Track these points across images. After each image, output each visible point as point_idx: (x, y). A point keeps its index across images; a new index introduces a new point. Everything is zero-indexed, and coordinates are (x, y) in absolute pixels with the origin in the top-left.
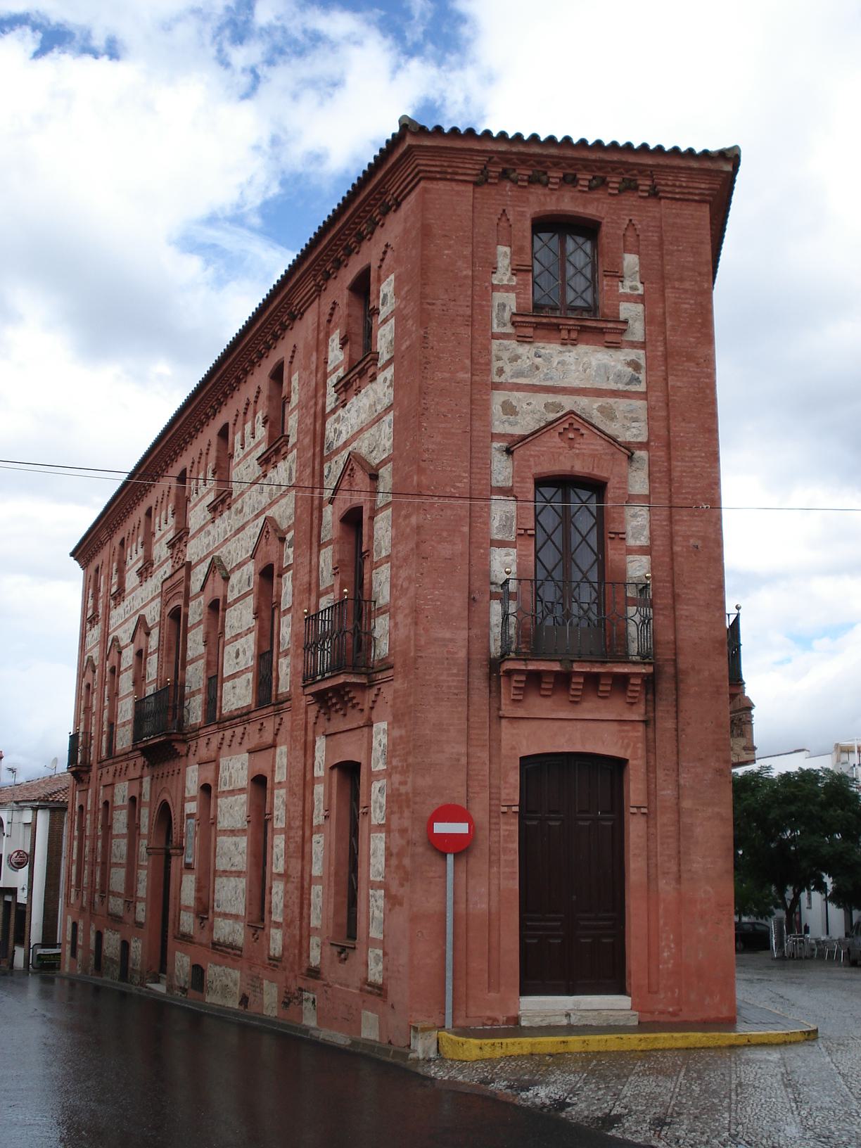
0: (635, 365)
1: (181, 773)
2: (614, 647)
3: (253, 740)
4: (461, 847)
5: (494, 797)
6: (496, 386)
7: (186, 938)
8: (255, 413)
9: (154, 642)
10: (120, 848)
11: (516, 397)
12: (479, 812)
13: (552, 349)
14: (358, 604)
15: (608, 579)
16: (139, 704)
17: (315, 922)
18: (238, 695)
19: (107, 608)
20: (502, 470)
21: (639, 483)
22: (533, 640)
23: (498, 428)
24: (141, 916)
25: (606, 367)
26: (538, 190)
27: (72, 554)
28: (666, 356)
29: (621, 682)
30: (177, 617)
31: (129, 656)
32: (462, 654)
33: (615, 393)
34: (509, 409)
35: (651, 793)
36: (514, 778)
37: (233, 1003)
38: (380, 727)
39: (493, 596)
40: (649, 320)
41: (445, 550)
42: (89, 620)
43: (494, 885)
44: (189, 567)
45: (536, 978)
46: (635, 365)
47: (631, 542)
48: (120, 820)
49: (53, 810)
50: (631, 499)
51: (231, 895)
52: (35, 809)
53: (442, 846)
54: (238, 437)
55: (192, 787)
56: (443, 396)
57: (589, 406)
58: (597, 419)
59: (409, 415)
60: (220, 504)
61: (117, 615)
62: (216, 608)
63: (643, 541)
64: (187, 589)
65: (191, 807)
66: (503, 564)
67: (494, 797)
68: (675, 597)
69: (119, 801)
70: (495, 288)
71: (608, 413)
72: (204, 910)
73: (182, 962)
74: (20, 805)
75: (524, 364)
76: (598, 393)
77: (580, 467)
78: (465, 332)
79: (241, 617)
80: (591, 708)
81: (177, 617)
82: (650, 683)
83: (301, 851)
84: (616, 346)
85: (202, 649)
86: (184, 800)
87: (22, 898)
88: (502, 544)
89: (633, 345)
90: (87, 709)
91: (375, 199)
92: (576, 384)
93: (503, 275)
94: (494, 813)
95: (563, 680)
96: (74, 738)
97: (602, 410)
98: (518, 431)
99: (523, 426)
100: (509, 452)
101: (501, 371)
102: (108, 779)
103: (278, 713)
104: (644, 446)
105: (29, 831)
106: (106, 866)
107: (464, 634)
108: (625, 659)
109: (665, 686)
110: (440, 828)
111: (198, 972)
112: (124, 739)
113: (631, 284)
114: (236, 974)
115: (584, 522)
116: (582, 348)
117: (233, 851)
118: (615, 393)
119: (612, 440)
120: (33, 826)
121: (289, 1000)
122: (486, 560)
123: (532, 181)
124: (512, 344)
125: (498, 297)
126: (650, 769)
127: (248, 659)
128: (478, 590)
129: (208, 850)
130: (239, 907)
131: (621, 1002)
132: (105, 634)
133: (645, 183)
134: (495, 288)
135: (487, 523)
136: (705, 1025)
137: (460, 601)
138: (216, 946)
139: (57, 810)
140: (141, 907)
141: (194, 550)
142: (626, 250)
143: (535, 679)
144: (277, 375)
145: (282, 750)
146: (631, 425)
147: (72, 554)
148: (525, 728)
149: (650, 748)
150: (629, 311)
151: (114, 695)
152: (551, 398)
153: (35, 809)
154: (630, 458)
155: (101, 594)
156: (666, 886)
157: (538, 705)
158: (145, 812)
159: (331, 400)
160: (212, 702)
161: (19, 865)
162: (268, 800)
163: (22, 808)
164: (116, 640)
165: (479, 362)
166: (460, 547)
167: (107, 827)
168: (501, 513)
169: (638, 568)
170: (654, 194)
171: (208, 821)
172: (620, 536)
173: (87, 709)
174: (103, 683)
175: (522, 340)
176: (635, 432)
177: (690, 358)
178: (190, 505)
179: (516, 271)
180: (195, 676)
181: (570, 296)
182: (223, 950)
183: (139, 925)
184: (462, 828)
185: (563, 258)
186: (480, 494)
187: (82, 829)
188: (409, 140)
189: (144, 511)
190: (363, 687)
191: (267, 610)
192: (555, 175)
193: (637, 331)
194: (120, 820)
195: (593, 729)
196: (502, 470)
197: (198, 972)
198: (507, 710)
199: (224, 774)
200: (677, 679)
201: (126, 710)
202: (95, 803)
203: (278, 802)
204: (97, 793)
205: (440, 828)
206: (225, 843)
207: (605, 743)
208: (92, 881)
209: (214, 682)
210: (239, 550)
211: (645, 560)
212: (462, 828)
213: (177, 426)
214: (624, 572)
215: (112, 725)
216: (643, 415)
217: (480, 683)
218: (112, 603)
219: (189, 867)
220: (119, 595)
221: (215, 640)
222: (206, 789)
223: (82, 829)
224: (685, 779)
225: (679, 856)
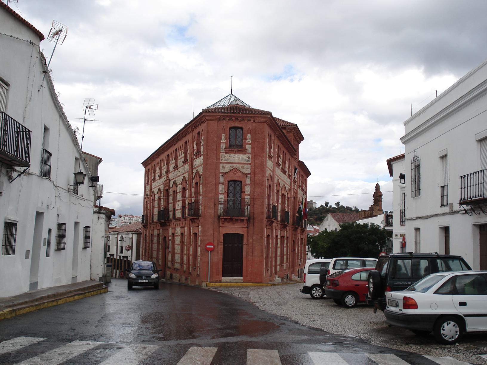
0: (249, 158)
1: (168, 230)
2: (242, 213)
3: (181, 225)
4: (212, 250)
5: (218, 241)
6: (221, 163)
7: (169, 268)
9: (162, 195)
10: (155, 246)
11: (225, 165)
12: (216, 244)
13: (232, 155)
14: (197, 202)
15: (242, 201)
16: (159, 212)
18: (179, 214)
20: (221, 179)
21: (248, 181)
22: (226, 212)
23: (221, 171)
24: (160, 263)
25: (243, 158)
26: (230, 121)
28: (255, 156)
29: (242, 220)
30: (167, 191)
31: (156, 198)
32: (213, 215)
33: (244, 164)
34: (223, 167)
35: (247, 241)
36: (222, 237)
37: (178, 281)
38: (200, 227)
39: (219, 204)
40: (252, 148)
41: (210, 195)
42: (146, 184)
43: (218, 257)
44: (170, 180)
45: (226, 273)
46: (249, 158)
47: (246, 193)
48: (155, 239)
49: (138, 234)
50: (247, 185)
51: (177, 258)
52: (133, 234)
53: (208, 250)
55: (170, 234)
56: (211, 163)
57: (239, 166)
58: (241, 169)
59: (205, 164)
60: (176, 167)
61: (154, 184)
62: (175, 192)
63: (249, 193)
64: (169, 186)
65: (170, 238)
66: (222, 198)
67: (218, 241)
68: (254, 204)
69: (155, 234)
70: (221, 143)
71: (243, 167)
72: (173, 261)
73: (168, 273)
74: (128, 233)
75: (227, 158)
76: (241, 163)
77: (237, 179)
78: (215, 152)
79: (179, 196)
80: (237, 225)
81: (167, 191)
82: (249, 220)
83: (189, 250)
84: (245, 154)
85: (172, 201)
86: (169, 236)
87: (129, 259)
88: (221, 194)
89: (248, 153)
90: (147, 208)
92: (237, 162)
93: (223, 140)
94: (218, 244)
95: (231, 220)
96: (143, 216)
97: (242, 167)
98: (225, 172)
99: (226, 170)
100: (223, 176)
101: (222, 160)
102: (152, 228)
103: (185, 220)
104: (249, 174)
105: (131, 240)
106: (152, 251)
107: (213, 211)
108: (244, 216)
109: (251, 221)
110: (208, 246)
111: (171, 275)
112: (156, 219)
113: (249, 141)
114: (178, 275)
115: (238, 188)
116: (238, 154)
117: (178, 248)
118: (244, 164)
119: (243, 173)
120: (132, 239)
121: (186, 279)
122: (218, 196)
123: (229, 120)
124: (224, 154)
125: (222, 144)
126: (248, 236)
127: (180, 207)
128: (217, 203)
129: (173, 248)
130: (179, 261)
131: (241, 278)
132: (151, 189)
133: (252, 120)
134: (221, 143)
135: (218, 190)
136: (258, 283)
137: (213, 205)
138: (175, 269)
139: (139, 234)
140: (160, 261)
141: (171, 176)
142: (248, 133)
143: (226, 219)
145: (186, 228)
146: (247, 169)
148: (224, 228)
149: (248, 232)
150: (248, 147)
151: (153, 206)
152: (232, 165)
153: (133, 234)
154: (247, 176)
156: (250, 258)
157: (227, 224)
158: (161, 238)
160: (174, 214)
161: (128, 250)
163: (128, 234)
164: (153, 192)
165: (218, 158)
166: (213, 194)
167: (152, 241)
168: (221, 187)
169: (247, 198)
170: (254, 121)
171: (173, 242)
172: (244, 192)
173: (147, 208)
174: (151, 202)
175: (226, 153)
176: (248, 171)
177: (260, 156)
179: (226, 139)
180: (171, 206)
181: (237, 142)
182: (176, 270)
183: (160, 265)
184: (212, 247)
185: (236, 135)
186: (217, 184)
187: (146, 241)
188: (204, 114)
190: (198, 219)
191: (184, 196)
192: (234, 119)
193: (249, 151)
194: (155, 239)
195: (237, 229)
196: (221, 179)
197: (171, 275)
198: (221, 225)
199: (176, 231)
200: (254, 220)
201: (156, 211)
202: (149, 234)
203: (185, 239)
204: (149, 231)
205: (208, 246)
206: (177, 247)
207: (239, 231)
208: (149, 255)
209: (175, 210)
210: (179, 180)
211: (249, 197)
212: (212, 247)
215: (153, 214)
216: (250, 168)
217: (216, 220)
219: (170, 252)
220: (154, 180)
221: (175, 200)
222: (173, 234)
223: (146, 241)
224: (254, 238)
225: (253, 252)
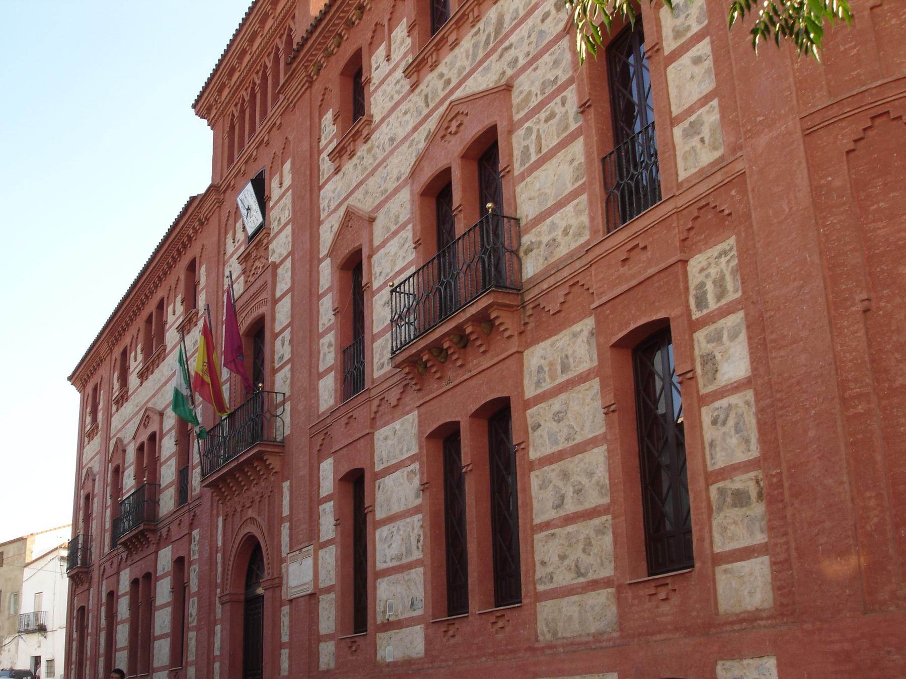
8: (175, 297)
17: (217, 653)
19: (109, 417)
27: (70, 379)
54: (133, 354)
91: (339, 18)
144: (192, 268)
147: (70, 379)
155: (100, 407)
159: (326, 166)
162: (186, 574)
178: (167, 326)
189: (121, 349)
213: (131, 297)
214: (473, 325)
218: (86, 439)
